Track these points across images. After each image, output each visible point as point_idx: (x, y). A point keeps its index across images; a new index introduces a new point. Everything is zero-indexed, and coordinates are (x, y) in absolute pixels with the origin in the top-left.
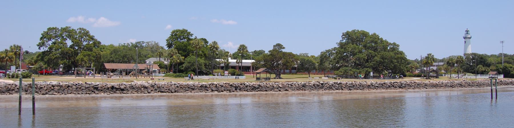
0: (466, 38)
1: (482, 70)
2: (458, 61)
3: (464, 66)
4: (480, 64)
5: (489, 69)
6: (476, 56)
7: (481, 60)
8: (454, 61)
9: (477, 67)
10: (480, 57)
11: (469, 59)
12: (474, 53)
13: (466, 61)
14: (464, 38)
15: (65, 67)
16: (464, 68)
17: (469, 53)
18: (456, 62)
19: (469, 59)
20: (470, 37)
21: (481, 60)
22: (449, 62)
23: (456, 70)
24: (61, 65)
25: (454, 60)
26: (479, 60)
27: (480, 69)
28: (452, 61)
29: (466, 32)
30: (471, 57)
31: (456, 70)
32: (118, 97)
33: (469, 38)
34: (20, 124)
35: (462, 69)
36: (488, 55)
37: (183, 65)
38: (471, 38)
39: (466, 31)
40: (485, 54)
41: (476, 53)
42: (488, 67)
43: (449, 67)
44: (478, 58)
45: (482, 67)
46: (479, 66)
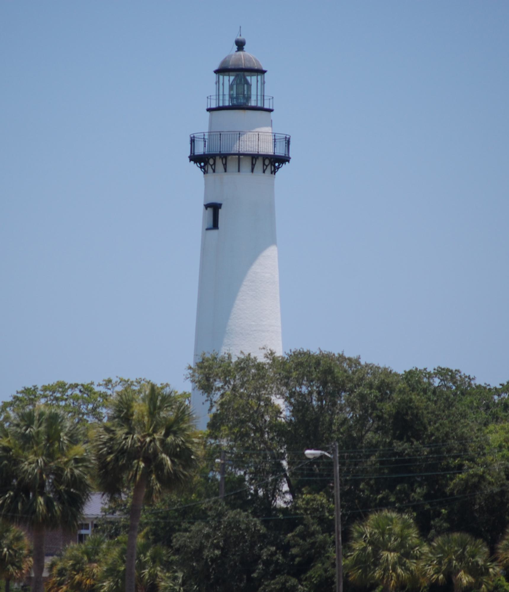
0: (225, 157)
1: (414, 579)
2: (122, 452)
3: (202, 516)
4: (383, 504)
5: (495, 570)
6: (342, 400)
7: (399, 446)
8: (80, 449)
9: (346, 536)
10: (387, 407)
11: (260, 430)
12: (315, 350)
13: (218, 451)
14: (195, 158)
15: (308, 409)
16: (199, 551)
17: (261, 359)
18: (103, 465)
19: (260, 430)
20: (267, 149)
21: (399, 446)
22: (16, 462)
23: (97, 569)
24: (384, 424)
25: (74, 440)
26: (373, 447)
27: (392, 556)
28: (50, 456)
29: (227, 80)
30: (279, 402)
31: (97, 569)
32: (249, 93)
33: (254, 157)
34: (240, 27)
35: (168, 566)
36: (480, 381)
37: (354, 380)
38: (284, 160)
39: (221, 71)
40: (442, 373)
41: (336, 351)
42: (476, 534)
43: (15, 530)
44: (362, 421)
45: (413, 534)
46: (373, 517)
